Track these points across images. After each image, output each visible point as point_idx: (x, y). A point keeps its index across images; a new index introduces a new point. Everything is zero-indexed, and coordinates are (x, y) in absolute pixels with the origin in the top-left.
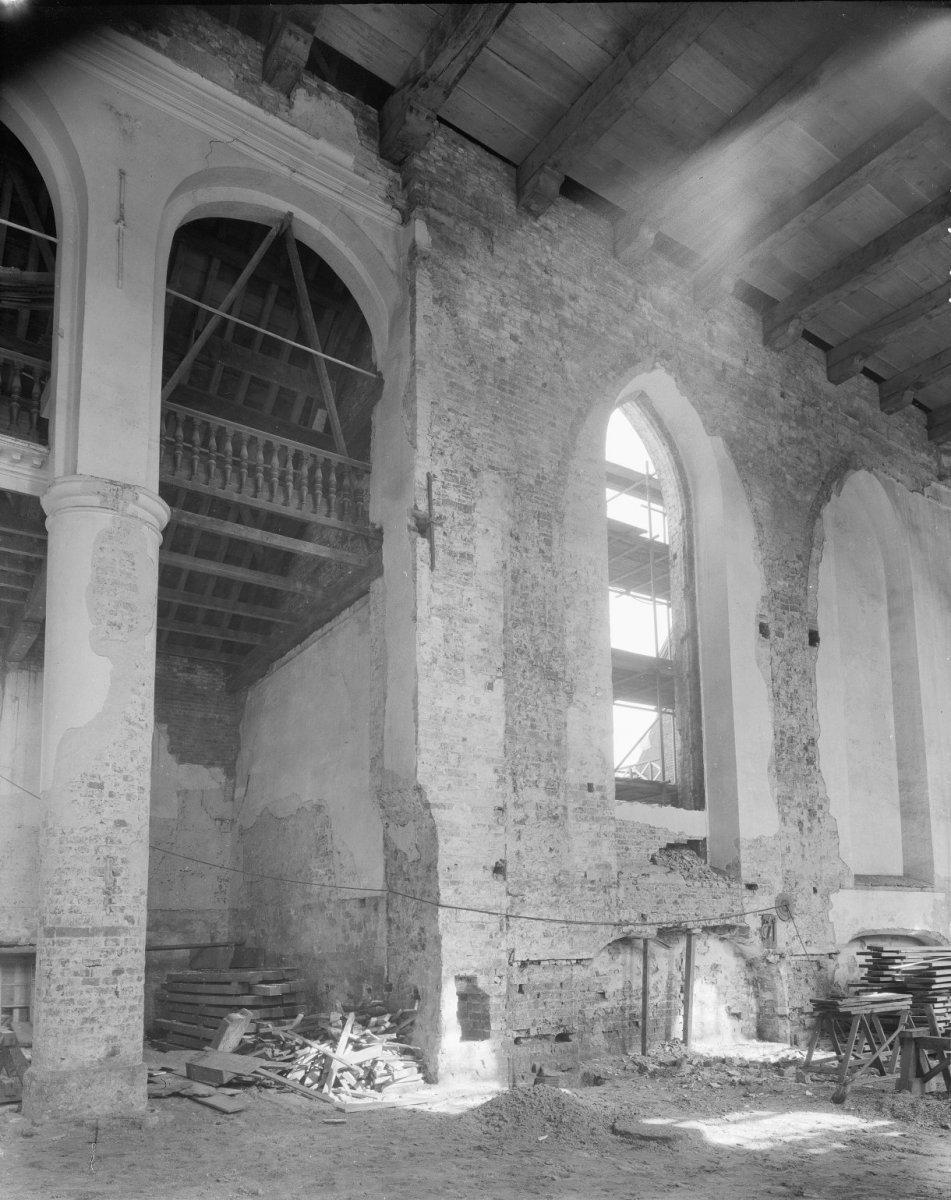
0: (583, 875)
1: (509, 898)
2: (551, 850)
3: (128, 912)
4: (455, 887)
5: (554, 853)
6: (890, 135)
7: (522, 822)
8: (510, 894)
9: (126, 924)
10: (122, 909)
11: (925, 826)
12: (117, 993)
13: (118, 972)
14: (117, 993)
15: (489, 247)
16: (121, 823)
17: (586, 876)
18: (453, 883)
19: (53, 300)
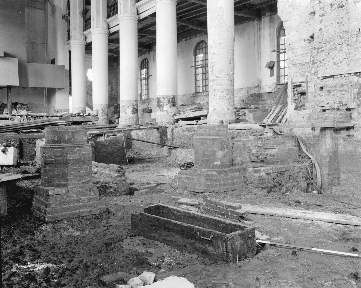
0: (358, 30)
1: (316, 50)
2: (338, 23)
3: (217, 75)
4: (293, 51)
5: (340, 24)
6: (35, 263)
7: (323, 15)
8: (316, 49)
9: (216, 78)
10: (215, 75)
11: (184, 6)
12: (214, 95)
13: (215, 90)
14: (214, 95)
15: (99, 152)
16: (214, 53)
17: (360, 30)
18: (292, 49)
19: (178, 30)
